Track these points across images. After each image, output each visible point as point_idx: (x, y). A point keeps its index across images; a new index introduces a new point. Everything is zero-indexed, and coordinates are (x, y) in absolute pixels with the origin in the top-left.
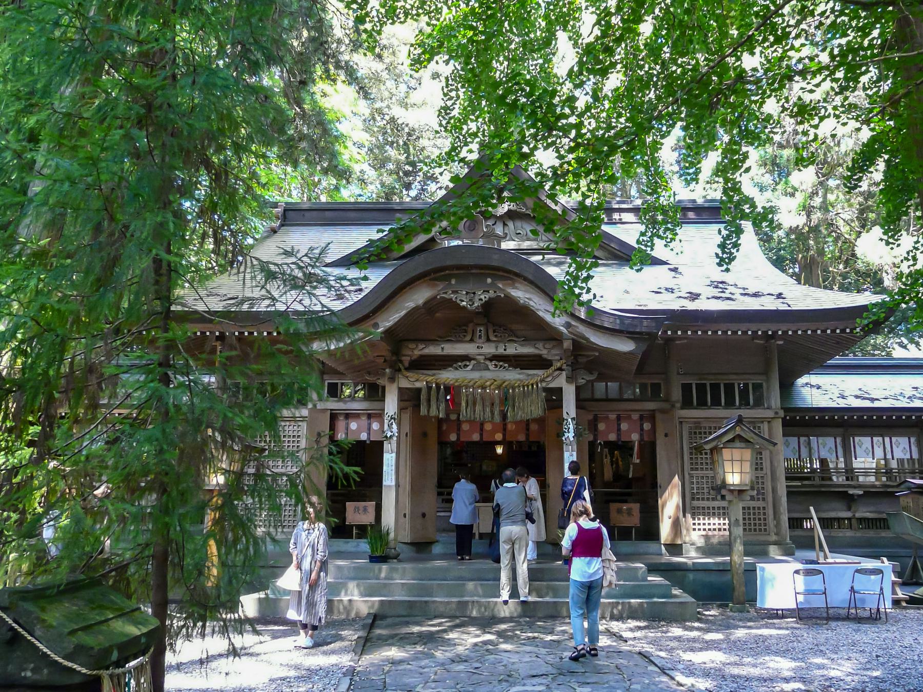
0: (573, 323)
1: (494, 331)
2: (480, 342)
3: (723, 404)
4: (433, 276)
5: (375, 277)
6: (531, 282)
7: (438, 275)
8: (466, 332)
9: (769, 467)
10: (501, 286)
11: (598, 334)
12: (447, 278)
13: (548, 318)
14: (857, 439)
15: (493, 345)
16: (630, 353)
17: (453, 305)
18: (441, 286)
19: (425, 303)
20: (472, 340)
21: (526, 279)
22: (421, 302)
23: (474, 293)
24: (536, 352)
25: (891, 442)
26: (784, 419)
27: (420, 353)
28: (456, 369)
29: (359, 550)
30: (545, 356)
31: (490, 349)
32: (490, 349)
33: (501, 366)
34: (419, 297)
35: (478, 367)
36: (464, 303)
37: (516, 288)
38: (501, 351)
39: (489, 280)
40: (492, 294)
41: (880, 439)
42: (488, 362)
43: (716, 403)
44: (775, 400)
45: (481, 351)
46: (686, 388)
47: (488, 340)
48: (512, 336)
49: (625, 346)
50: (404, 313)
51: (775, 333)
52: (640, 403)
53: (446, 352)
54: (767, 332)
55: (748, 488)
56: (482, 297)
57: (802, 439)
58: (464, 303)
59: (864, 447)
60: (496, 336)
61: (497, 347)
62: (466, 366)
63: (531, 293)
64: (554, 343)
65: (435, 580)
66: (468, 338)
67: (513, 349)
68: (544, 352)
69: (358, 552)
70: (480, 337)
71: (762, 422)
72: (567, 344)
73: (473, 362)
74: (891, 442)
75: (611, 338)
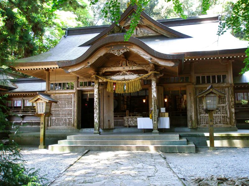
0: (153, 58)
1: (129, 63)
2: (124, 67)
3: (211, 82)
4: (106, 46)
5: (86, 49)
6: (138, 46)
7: (107, 46)
8: (119, 63)
9: (73, 114)
10: (128, 48)
11: (161, 61)
12: (111, 46)
13: (144, 57)
14: (238, 94)
15: (129, 67)
16: (173, 67)
17: (113, 55)
18: (109, 49)
19: (104, 55)
20: (121, 66)
21: (136, 45)
22: (102, 54)
23: (120, 51)
24: (143, 68)
25: (237, 95)
26: (234, 87)
27: (105, 71)
28: (117, 75)
29: (91, 131)
30: (146, 70)
31: (127, 68)
32: (127, 68)
33: (131, 74)
34: (102, 53)
35: (124, 74)
36: (116, 54)
37: (134, 48)
38: (131, 69)
39: (124, 46)
40: (125, 50)
41: (242, 94)
42: (127, 73)
43: (203, 82)
44: (230, 79)
45: (124, 69)
46: (198, 78)
47: (127, 65)
48: (135, 63)
49: (171, 64)
50: (97, 58)
51: (229, 58)
52: (177, 84)
53: (113, 70)
54: (226, 57)
55: (215, 109)
56: (122, 52)
57: (245, 93)
58: (116, 54)
59: (241, 96)
60: (129, 64)
61: (129, 68)
62: (120, 74)
63: (138, 49)
64: (148, 65)
65: (75, 146)
66: (120, 65)
67: (135, 68)
68: (145, 69)
69: (90, 132)
70: (124, 65)
71: (226, 88)
72: (151, 65)
73: (122, 73)
74: (12, 105)
75: (166, 62)
